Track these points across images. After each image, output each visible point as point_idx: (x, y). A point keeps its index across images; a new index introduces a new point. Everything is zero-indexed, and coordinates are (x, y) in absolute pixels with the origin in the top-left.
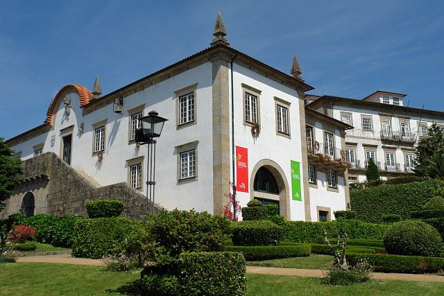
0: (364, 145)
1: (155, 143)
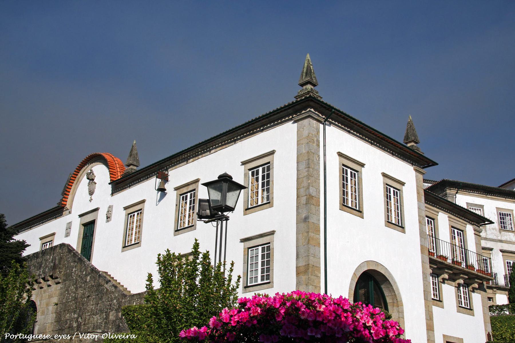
0: (502, 251)
1: (227, 219)
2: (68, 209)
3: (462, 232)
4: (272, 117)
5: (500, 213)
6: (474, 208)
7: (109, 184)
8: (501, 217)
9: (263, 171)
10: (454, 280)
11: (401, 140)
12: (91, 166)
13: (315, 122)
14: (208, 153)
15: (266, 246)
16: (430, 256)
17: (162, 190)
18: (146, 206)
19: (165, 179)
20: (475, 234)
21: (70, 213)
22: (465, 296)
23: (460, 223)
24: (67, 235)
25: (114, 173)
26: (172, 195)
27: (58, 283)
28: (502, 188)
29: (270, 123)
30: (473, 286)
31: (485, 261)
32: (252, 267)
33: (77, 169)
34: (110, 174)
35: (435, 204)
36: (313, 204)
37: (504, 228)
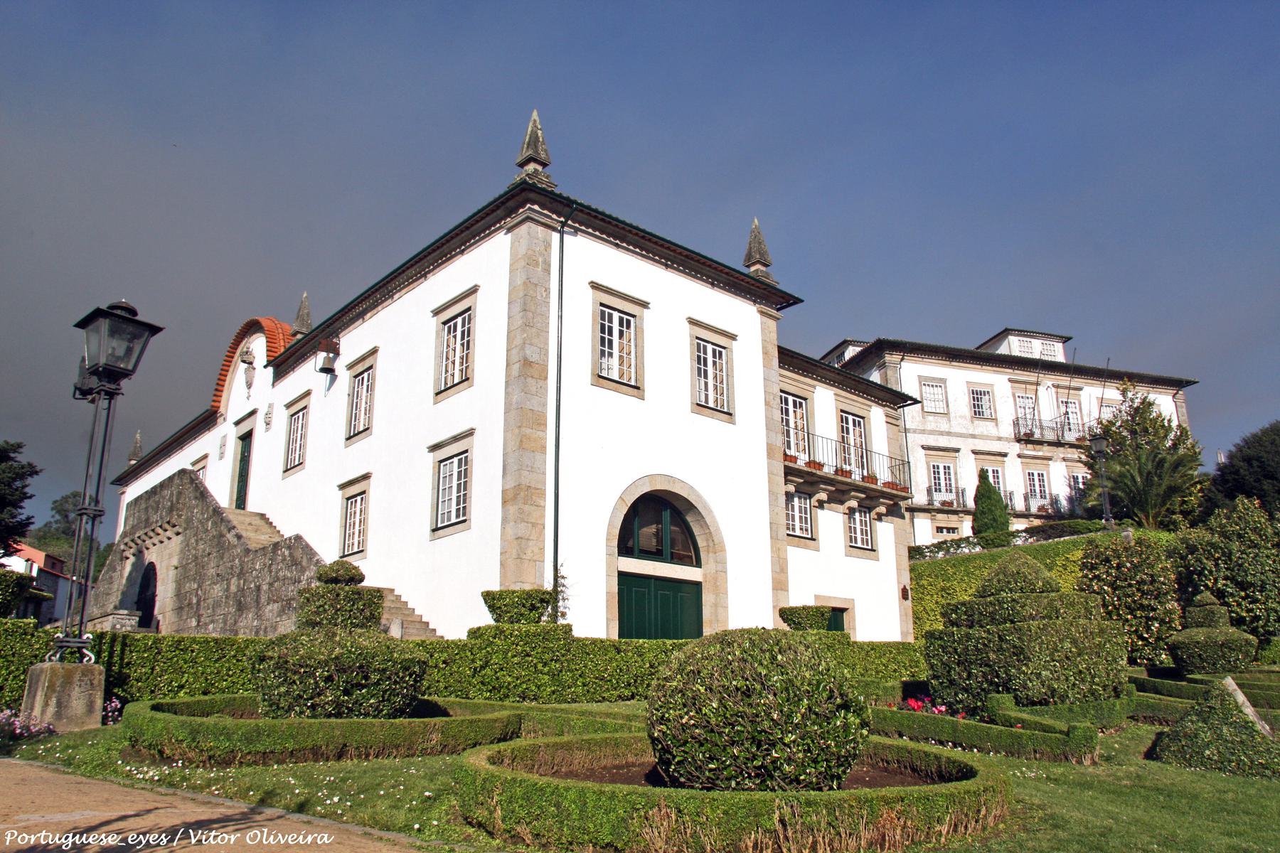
0: (974, 452)
2: (222, 415)
3: (860, 420)
4: (475, 227)
5: (973, 391)
6: (931, 384)
8: (974, 398)
10: (842, 503)
11: (737, 263)
13: (540, 229)
14: (390, 301)
16: (787, 463)
17: (328, 370)
18: (313, 401)
20: (887, 422)
22: (864, 528)
23: (858, 405)
25: (273, 349)
27: (178, 534)
28: (982, 351)
29: (474, 237)
30: (878, 510)
31: (902, 464)
32: (444, 496)
33: (230, 347)
35: (808, 372)
36: (532, 377)
37: (979, 415)
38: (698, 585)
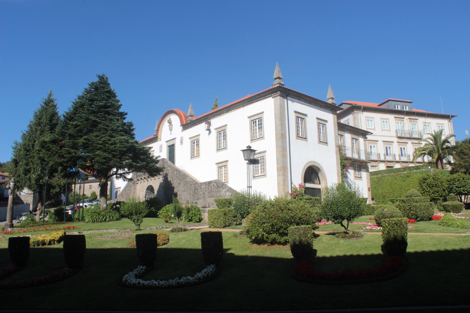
7: (180, 126)
9: (259, 122)
12: (169, 115)
15: (262, 158)
17: (209, 130)
19: (209, 124)
21: (160, 140)
24: (161, 151)
26: (214, 133)
34: (180, 121)
38: (320, 189)
